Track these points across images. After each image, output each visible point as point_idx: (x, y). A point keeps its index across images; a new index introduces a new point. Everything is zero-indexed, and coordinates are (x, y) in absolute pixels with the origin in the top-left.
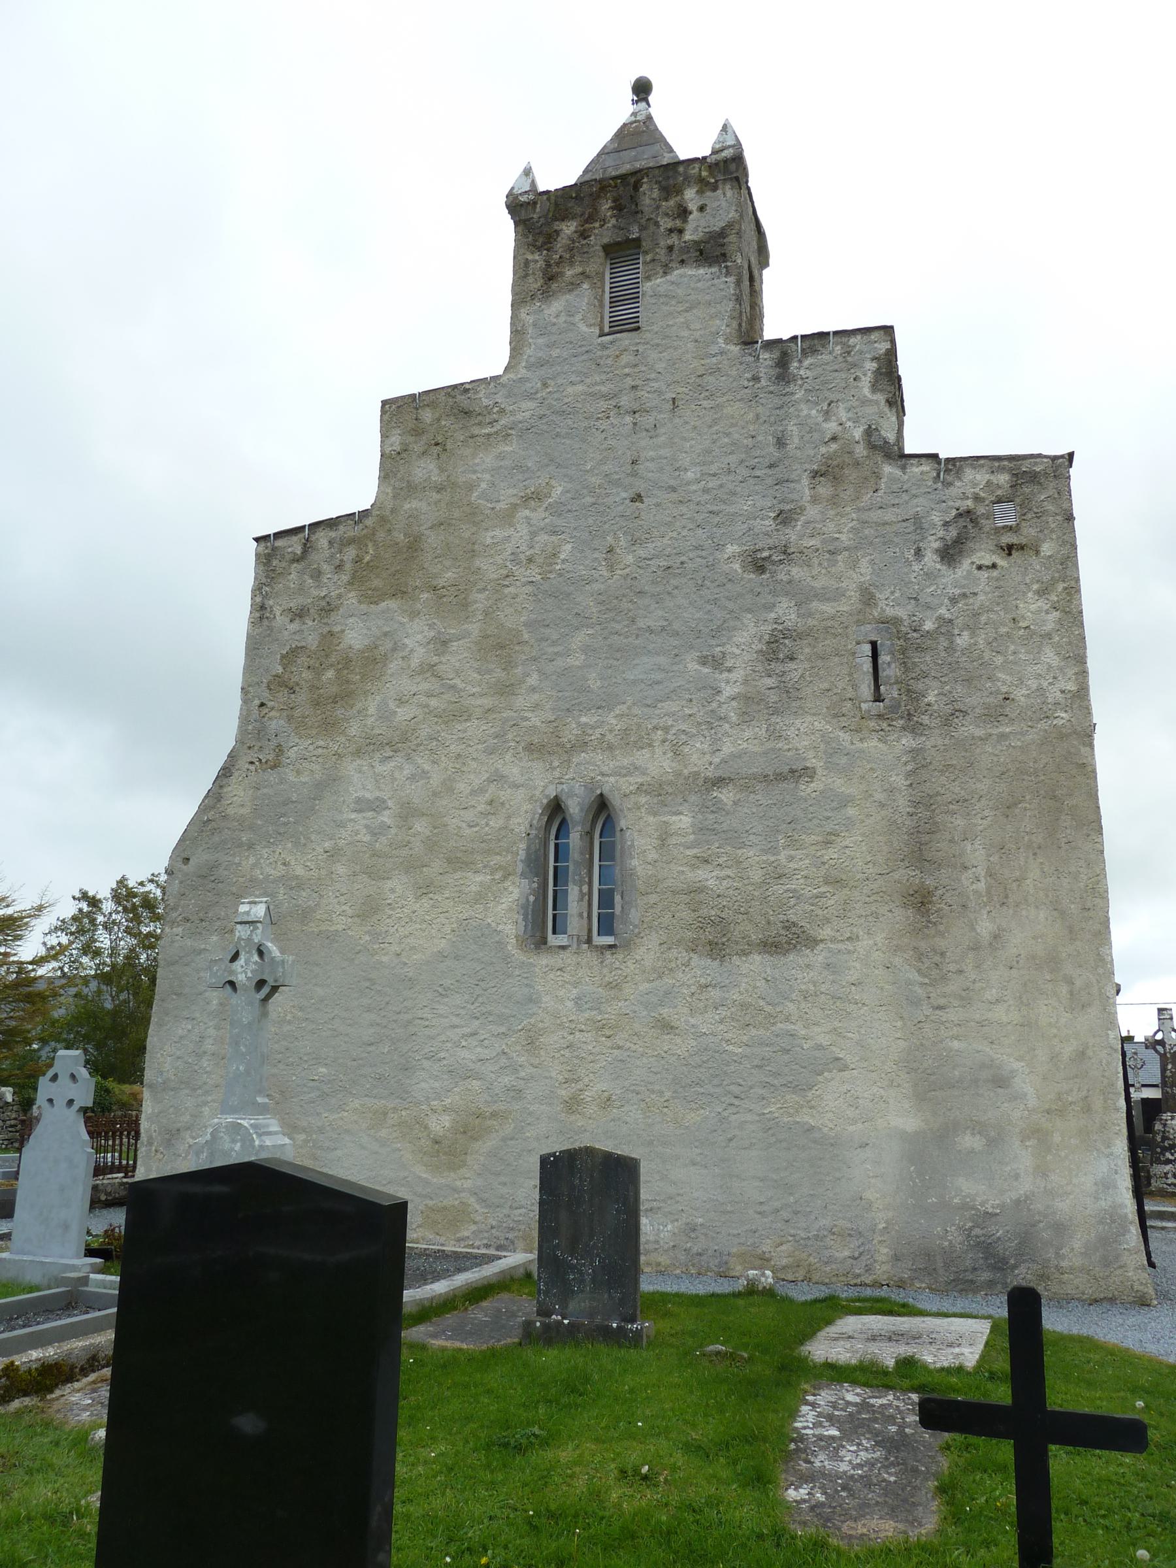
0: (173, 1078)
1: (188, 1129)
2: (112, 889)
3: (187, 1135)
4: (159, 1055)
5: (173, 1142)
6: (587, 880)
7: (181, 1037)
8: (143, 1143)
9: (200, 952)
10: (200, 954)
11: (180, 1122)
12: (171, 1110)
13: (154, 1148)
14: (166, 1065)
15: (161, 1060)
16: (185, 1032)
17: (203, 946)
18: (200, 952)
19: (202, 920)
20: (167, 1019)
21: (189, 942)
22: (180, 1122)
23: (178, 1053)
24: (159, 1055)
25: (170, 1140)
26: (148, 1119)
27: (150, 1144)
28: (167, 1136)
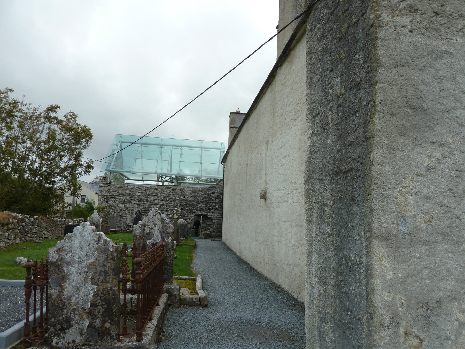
0: (424, 226)
1: (453, 299)
2: (47, 133)
3: (454, 307)
4: (396, 193)
5: (434, 319)
6: (33, 308)
7: (428, 169)
8: (381, 324)
9: (440, 55)
10: (440, 57)
11: (440, 290)
12: (425, 272)
13: (402, 330)
14: (409, 207)
15: (401, 199)
16: (433, 162)
17: (445, 48)
18: (440, 55)
19: (437, 14)
20: (402, 140)
21: (422, 40)
22: (440, 290)
23: (425, 191)
24: (396, 193)
25: (428, 317)
26: (389, 287)
27: (395, 323)
28: (423, 312)
